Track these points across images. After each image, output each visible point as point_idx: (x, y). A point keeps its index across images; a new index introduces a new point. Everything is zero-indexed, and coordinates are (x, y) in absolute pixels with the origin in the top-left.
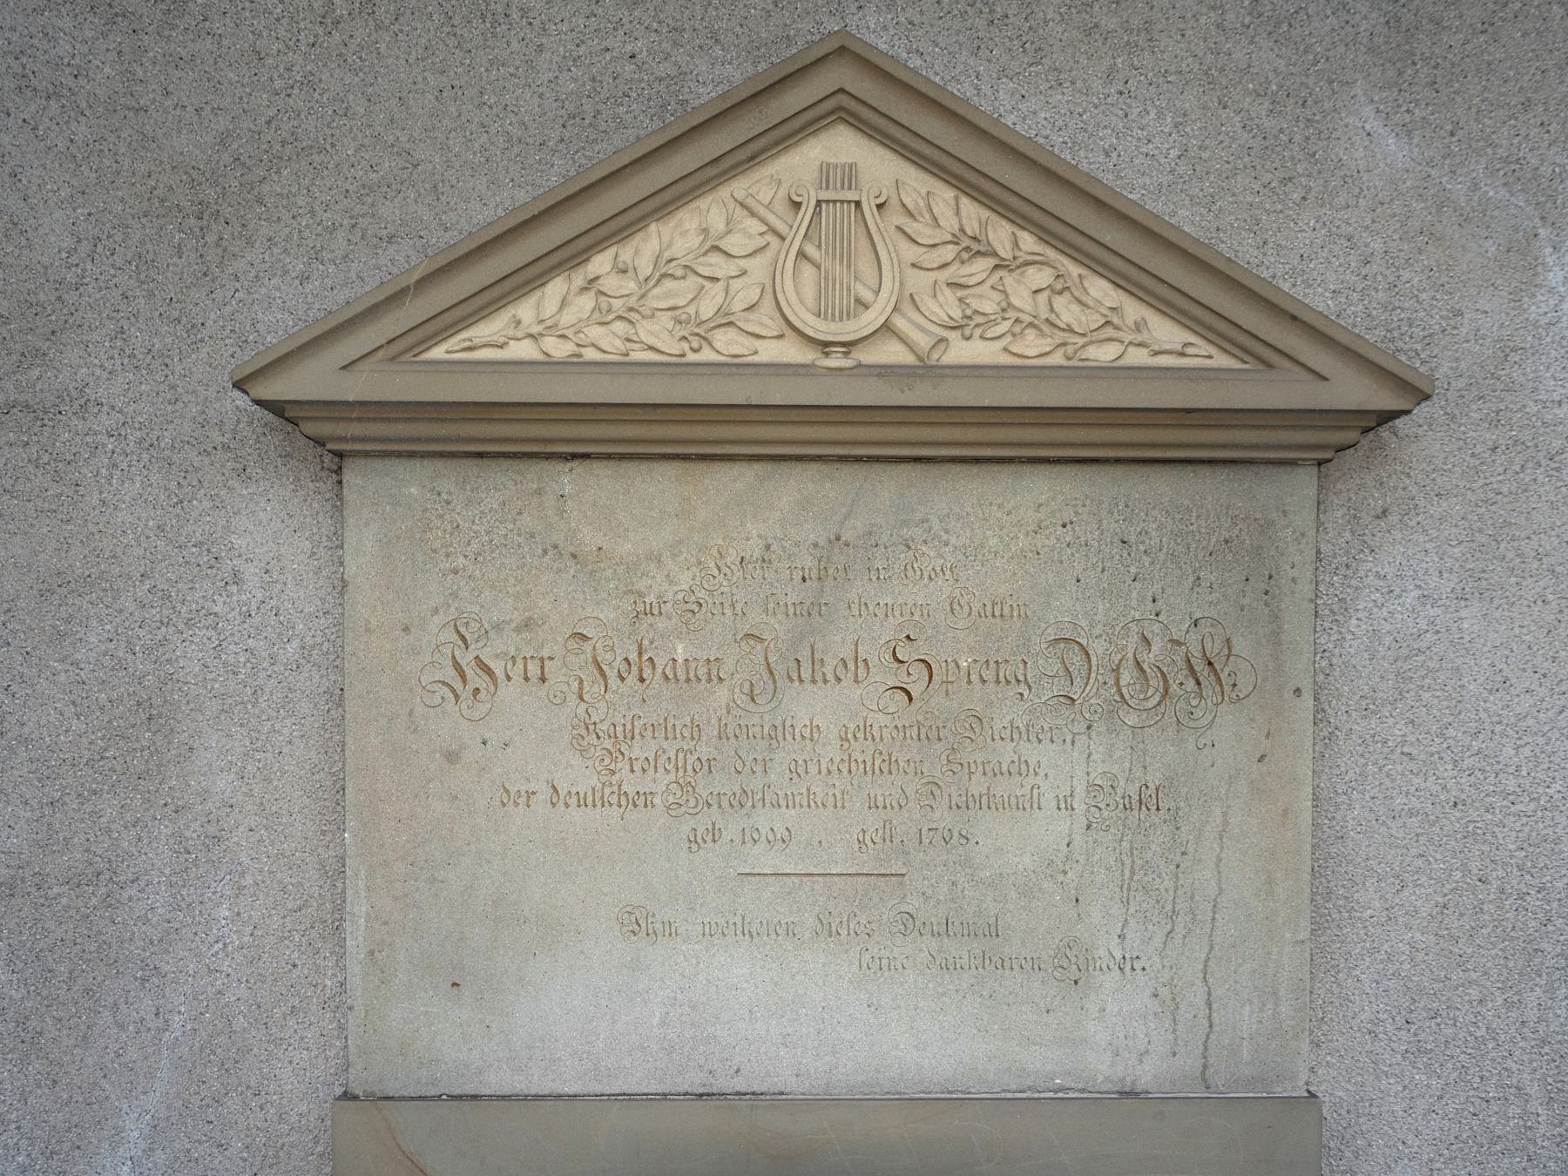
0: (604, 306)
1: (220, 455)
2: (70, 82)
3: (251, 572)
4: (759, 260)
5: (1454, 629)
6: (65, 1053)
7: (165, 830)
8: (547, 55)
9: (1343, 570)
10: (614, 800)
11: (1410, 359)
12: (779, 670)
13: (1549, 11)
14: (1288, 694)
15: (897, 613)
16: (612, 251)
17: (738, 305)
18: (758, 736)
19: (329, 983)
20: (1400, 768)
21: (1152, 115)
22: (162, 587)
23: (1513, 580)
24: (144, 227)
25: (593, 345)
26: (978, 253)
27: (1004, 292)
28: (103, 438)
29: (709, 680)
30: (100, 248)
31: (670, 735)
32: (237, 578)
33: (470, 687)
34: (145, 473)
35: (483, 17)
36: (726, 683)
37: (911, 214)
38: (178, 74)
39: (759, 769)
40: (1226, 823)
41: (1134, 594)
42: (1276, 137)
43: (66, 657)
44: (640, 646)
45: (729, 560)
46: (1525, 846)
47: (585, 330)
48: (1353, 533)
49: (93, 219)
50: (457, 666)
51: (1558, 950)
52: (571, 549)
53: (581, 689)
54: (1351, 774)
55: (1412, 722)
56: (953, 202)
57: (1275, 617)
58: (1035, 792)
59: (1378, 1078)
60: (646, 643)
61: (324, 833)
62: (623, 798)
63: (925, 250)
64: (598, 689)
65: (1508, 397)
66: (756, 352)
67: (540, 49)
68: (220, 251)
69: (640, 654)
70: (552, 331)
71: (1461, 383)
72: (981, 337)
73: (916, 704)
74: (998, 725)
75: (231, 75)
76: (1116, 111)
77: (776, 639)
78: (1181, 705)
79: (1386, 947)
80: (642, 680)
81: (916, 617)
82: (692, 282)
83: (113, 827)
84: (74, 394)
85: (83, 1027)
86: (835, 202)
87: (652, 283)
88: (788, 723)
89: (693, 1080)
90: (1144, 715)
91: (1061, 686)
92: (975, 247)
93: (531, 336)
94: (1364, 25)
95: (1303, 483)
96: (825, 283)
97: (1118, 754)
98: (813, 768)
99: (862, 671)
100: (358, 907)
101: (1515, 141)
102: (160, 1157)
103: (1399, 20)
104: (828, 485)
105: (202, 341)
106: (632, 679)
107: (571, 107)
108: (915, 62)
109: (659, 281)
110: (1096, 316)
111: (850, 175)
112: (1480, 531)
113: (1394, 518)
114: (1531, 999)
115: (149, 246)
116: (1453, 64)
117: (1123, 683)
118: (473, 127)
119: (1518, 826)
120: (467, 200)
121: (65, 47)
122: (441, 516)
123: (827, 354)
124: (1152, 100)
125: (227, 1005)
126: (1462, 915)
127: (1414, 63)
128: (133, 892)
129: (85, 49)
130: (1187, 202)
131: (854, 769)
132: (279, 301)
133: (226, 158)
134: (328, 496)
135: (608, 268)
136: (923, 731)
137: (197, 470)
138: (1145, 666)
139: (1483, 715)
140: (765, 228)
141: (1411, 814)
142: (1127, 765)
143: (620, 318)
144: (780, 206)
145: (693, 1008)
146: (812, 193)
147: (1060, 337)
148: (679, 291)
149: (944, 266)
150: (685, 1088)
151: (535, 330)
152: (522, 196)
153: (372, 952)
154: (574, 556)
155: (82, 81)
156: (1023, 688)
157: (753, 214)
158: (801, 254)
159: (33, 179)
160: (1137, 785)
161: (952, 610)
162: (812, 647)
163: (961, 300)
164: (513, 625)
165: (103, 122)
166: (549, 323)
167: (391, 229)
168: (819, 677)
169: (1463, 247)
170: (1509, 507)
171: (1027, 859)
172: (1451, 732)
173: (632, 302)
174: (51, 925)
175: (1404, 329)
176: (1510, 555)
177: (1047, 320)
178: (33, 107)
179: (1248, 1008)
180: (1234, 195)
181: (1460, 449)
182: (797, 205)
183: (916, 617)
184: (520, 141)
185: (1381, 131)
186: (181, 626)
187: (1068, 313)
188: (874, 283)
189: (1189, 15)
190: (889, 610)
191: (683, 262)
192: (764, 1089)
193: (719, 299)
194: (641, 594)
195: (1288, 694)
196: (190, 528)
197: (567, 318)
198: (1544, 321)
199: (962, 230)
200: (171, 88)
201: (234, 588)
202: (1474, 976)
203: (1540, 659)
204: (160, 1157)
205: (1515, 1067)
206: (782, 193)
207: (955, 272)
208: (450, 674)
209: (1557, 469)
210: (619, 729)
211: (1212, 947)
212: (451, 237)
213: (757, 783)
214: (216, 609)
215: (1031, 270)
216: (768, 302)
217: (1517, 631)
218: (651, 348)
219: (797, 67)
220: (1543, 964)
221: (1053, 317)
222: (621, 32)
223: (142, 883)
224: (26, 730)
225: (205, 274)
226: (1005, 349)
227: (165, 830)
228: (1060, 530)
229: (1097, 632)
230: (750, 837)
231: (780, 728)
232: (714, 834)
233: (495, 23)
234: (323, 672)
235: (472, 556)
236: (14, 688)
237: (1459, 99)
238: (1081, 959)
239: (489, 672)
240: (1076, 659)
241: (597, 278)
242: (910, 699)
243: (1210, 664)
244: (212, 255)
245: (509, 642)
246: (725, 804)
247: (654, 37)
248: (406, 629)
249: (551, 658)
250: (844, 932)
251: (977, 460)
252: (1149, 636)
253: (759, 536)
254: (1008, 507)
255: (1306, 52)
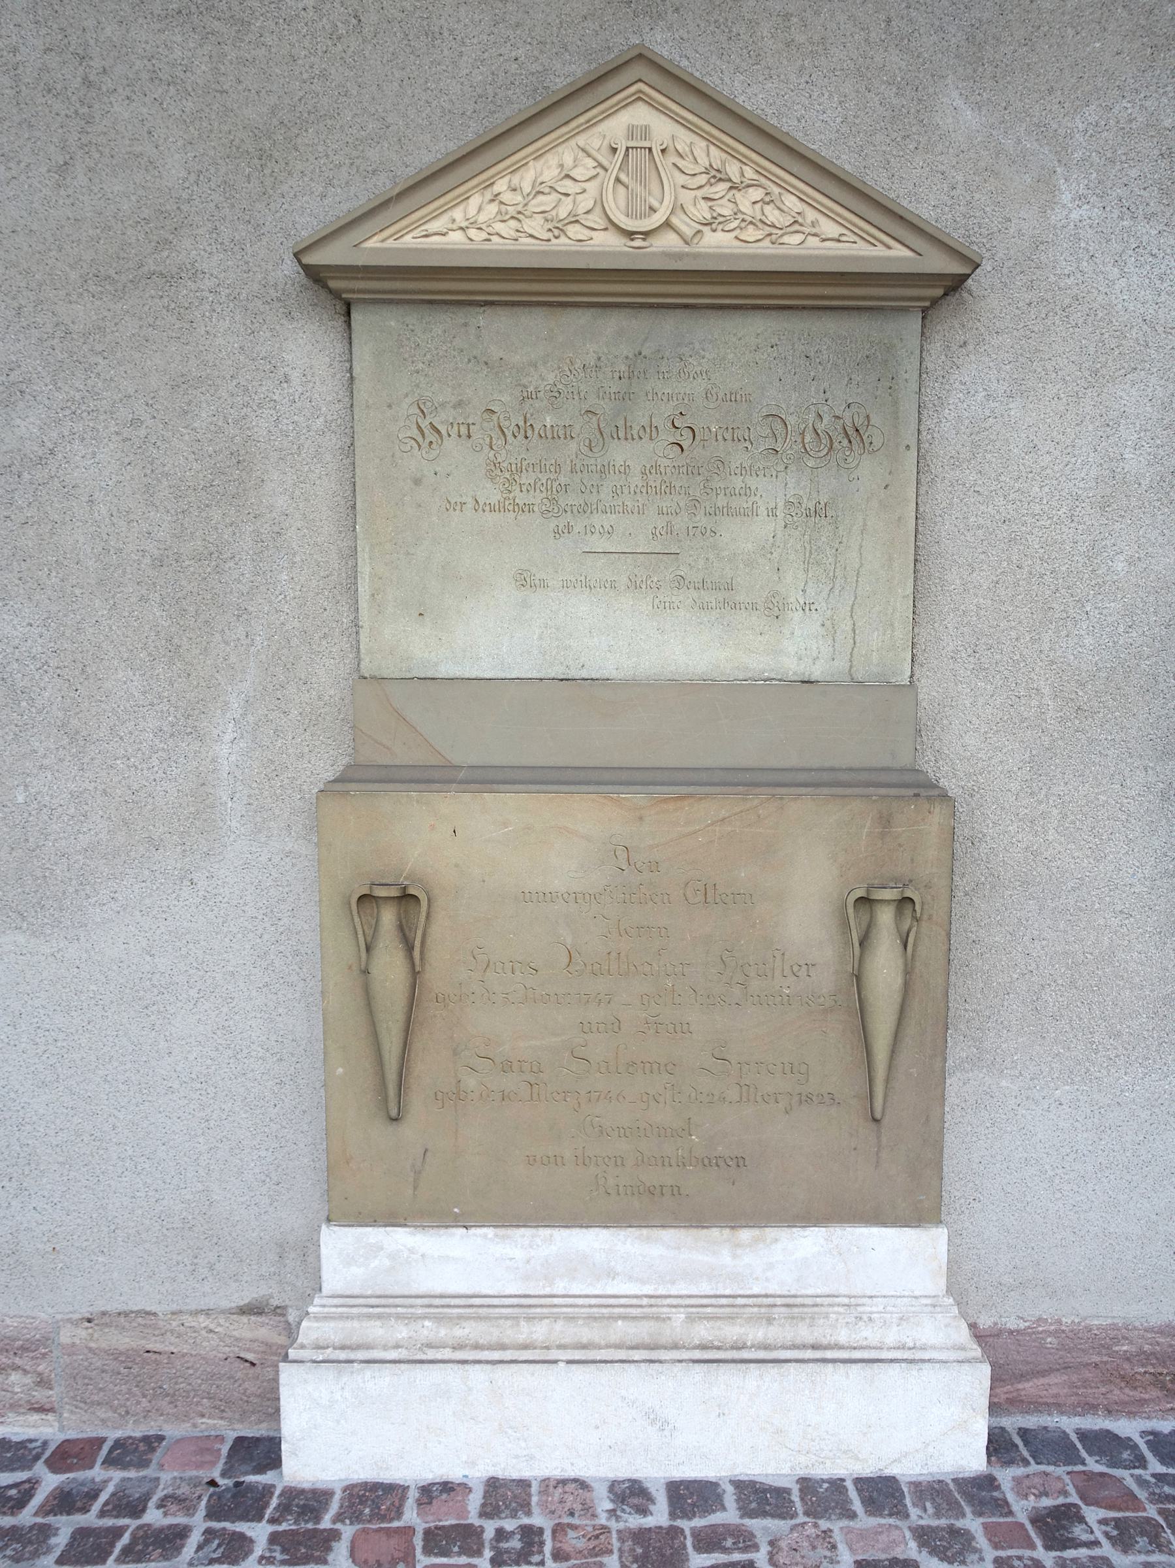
0: (503, 210)
1: (277, 304)
2: (182, 75)
3: (295, 376)
4: (594, 184)
5: (1006, 416)
6: (195, 658)
7: (249, 528)
8: (465, 58)
9: (940, 379)
10: (511, 508)
11: (979, 248)
12: (606, 431)
13: (1065, 31)
14: (902, 448)
15: (675, 399)
16: (507, 179)
17: (581, 210)
18: (594, 471)
19: (345, 620)
20: (972, 500)
21: (826, 96)
22: (242, 384)
23: (1041, 385)
24: (227, 164)
25: (498, 234)
26: (720, 180)
27: (735, 203)
28: (207, 294)
29: (566, 438)
30: (201, 178)
31: (543, 470)
32: (287, 379)
33: (427, 441)
34: (232, 314)
35: (427, 35)
36: (576, 439)
37: (681, 156)
38: (246, 69)
39: (594, 490)
40: (865, 525)
41: (813, 389)
42: (900, 110)
43: (188, 425)
44: (525, 418)
45: (576, 366)
46: (1044, 546)
47: (493, 225)
48: (946, 356)
49: (197, 159)
50: (419, 427)
51: (1062, 608)
52: (485, 359)
53: (491, 443)
54: (944, 504)
55: (980, 472)
56: (705, 148)
57: (895, 403)
58: (755, 506)
59: (956, 684)
60: (528, 415)
61: (340, 532)
62: (516, 507)
63: (689, 177)
64: (501, 442)
65: (1038, 272)
66: (592, 239)
67: (461, 54)
68: (272, 179)
69: (525, 422)
70: (473, 226)
71: (1010, 263)
72: (723, 230)
73: (686, 453)
74: (733, 467)
75: (277, 70)
76: (803, 93)
77: (604, 413)
78: (840, 455)
79: (962, 607)
80: (526, 437)
81: (686, 402)
82: (554, 196)
83: (218, 526)
84: (189, 266)
85: (204, 643)
86: (637, 148)
87: (531, 197)
88: (612, 463)
89: (557, 671)
90: (818, 460)
91: (770, 443)
92: (719, 176)
93: (461, 228)
94: (954, 40)
95: (914, 323)
96: (631, 197)
97: (803, 483)
98: (626, 491)
99: (654, 434)
100: (365, 569)
101: (1044, 113)
102: (251, 718)
103: (974, 37)
104: (634, 321)
105: (263, 234)
106: (520, 437)
107: (479, 91)
108: (684, 63)
109: (535, 196)
110: (789, 218)
111: (646, 132)
112: (1021, 355)
113: (971, 347)
114: (1046, 638)
115: (230, 176)
116: (1007, 65)
117: (806, 441)
118: (422, 103)
119: (1040, 534)
120: (419, 149)
121: (178, 53)
122: (409, 339)
123: (632, 240)
124: (826, 87)
125: (286, 631)
126: (1007, 588)
127: (983, 65)
128: (232, 564)
129: (190, 54)
130: (847, 150)
131: (649, 491)
132: (308, 210)
133: (275, 122)
134: (339, 329)
135: (505, 188)
136: (690, 469)
137: (262, 313)
138: (819, 432)
139: (1021, 467)
140: (596, 164)
141: (979, 527)
142: (808, 490)
143: (513, 217)
144: (605, 150)
145: (558, 629)
146: (623, 142)
147: (768, 230)
148: (546, 202)
149: (700, 187)
150: (552, 675)
151: (464, 224)
152: (452, 146)
153: (373, 595)
154: (486, 363)
155: (189, 74)
156: (748, 444)
157: (589, 155)
158: (618, 180)
159: (161, 135)
160: (814, 502)
161: (707, 397)
162: (625, 418)
163: (710, 207)
164: (451, 404)
165: (201, 99)
166: (471, 221)
167: (374, 166)
168: (629, 436)
169: (1011, 179)
170: (1039, 340)
171: (750, 545)
172: (1003, 478)
173: (520, 208)
174: (184, 583)
175: (976, 229)
176: (1039, 370)
177: (760, 220)
178: (160, 90)
179: (876, 633)
180: (875, 146)
181: (1010, 304)
182: (614, 150)
183: (686, 402)
184: (450, 112)
185: (963, 106)
186: (255, 408)
187: (772, 215)
188: (659, 196)
189: (848, 34)
190: (670, 397)
191: (549, 184)
192: (598, 677)
193: (570, 207)
194: (525, 387)
195: (902, 448)
196: (258, 348)
197: (482, 218)
198: (1059, 225)
199: (711, 166)
200: (242, 78)
201: (285, 385)
202: (1013, 624)
203: (1055, 433)
204: (251, 718)
205: (1035, 678)
206: (606, 143)
207: (708, 191)
208: (415, 432)
209: (1067, 317)
210: (514, 466)
211: (856, 598)
212: (411, 171)
213: (593, 499)
214: (275, 398)
215: (751, 190)
216: (598, 209)
217: (1042, 416)
218: (531, 236)
219: (615, 65)
220: (1053, 616)
221: (763, 218)
222: (509, 44)
223: (237, 559)
224: (166, 468)
225: (264, 194)
226: (736, 238)
227: (249, 528)
228: (770, 350)
229: (791, 410)
230: (590, 530)
231: (607, 467)
232: (569, 528)
233: (434, 39)
234: (338, 436)
235: (427, 363)
236: (158, 444)
237: (1010, 87)
238: (781, 603)
239: (438, 432)
240: (779, 426)
241: (499, 194)
242: (682, 450)
243: (857, 430)
244: (268, 182)
245: (448, 414)
246: (575, 511)
247: (528, 47)
248: (390, 406)
249: (473, 424)
250: (644, 587)
251: (721, 307)
252: (821, 414)
253: (594, 352)
254: (740, 335)
255: (918, 57)
